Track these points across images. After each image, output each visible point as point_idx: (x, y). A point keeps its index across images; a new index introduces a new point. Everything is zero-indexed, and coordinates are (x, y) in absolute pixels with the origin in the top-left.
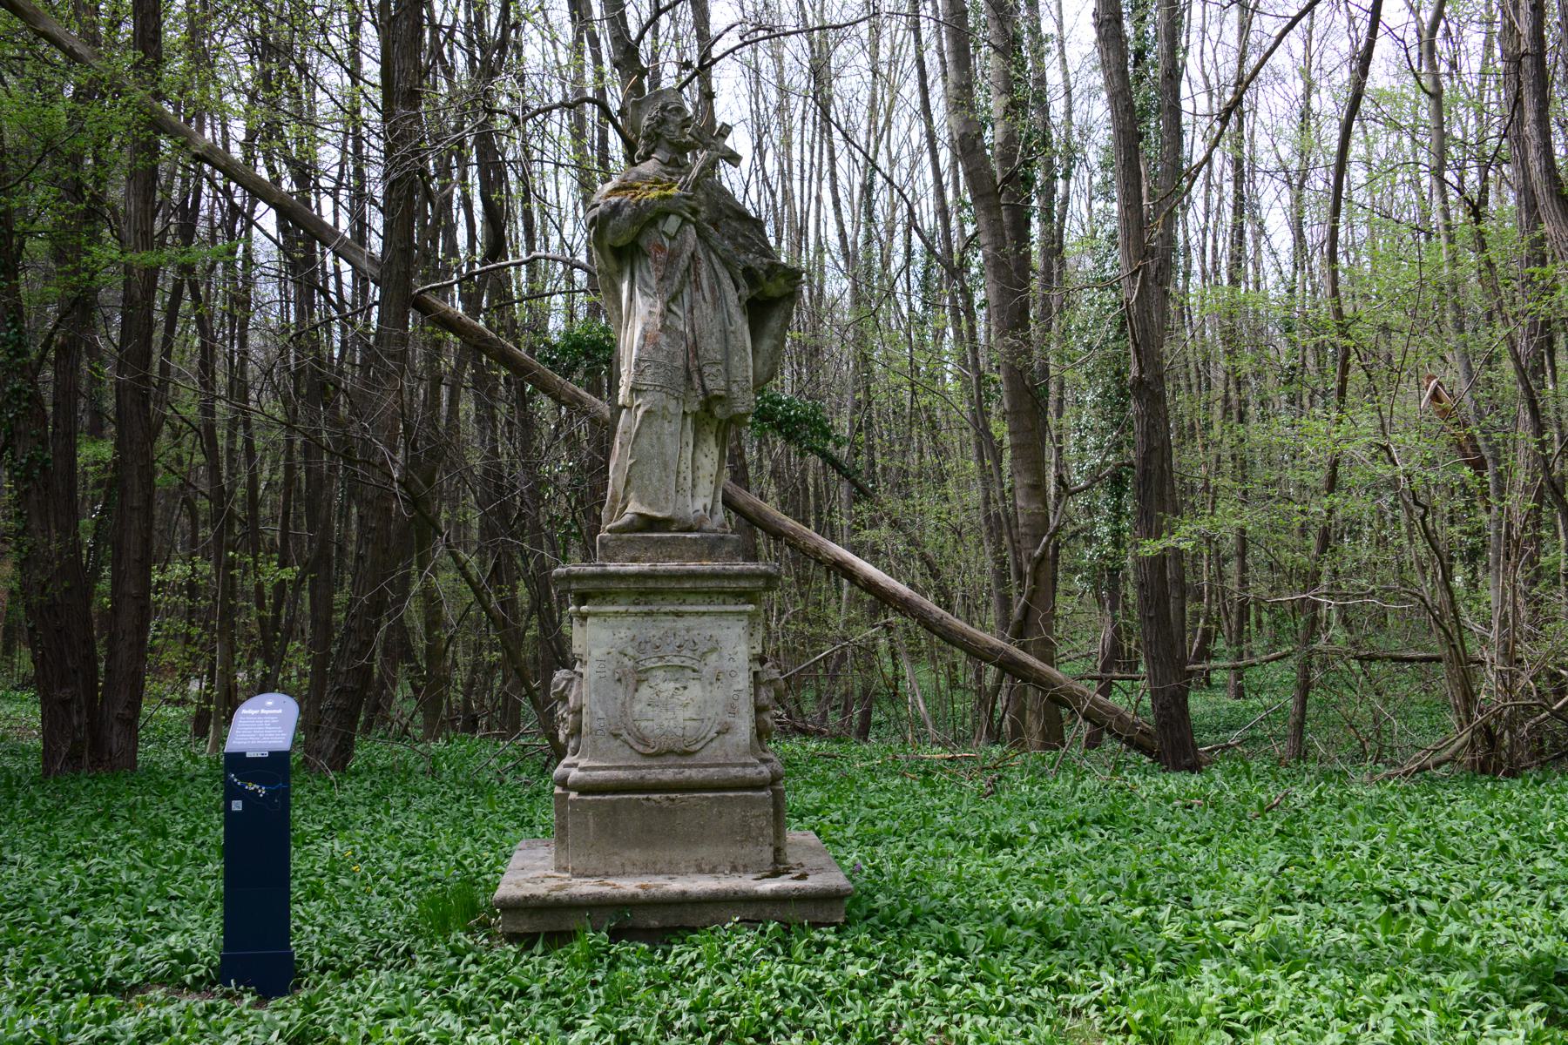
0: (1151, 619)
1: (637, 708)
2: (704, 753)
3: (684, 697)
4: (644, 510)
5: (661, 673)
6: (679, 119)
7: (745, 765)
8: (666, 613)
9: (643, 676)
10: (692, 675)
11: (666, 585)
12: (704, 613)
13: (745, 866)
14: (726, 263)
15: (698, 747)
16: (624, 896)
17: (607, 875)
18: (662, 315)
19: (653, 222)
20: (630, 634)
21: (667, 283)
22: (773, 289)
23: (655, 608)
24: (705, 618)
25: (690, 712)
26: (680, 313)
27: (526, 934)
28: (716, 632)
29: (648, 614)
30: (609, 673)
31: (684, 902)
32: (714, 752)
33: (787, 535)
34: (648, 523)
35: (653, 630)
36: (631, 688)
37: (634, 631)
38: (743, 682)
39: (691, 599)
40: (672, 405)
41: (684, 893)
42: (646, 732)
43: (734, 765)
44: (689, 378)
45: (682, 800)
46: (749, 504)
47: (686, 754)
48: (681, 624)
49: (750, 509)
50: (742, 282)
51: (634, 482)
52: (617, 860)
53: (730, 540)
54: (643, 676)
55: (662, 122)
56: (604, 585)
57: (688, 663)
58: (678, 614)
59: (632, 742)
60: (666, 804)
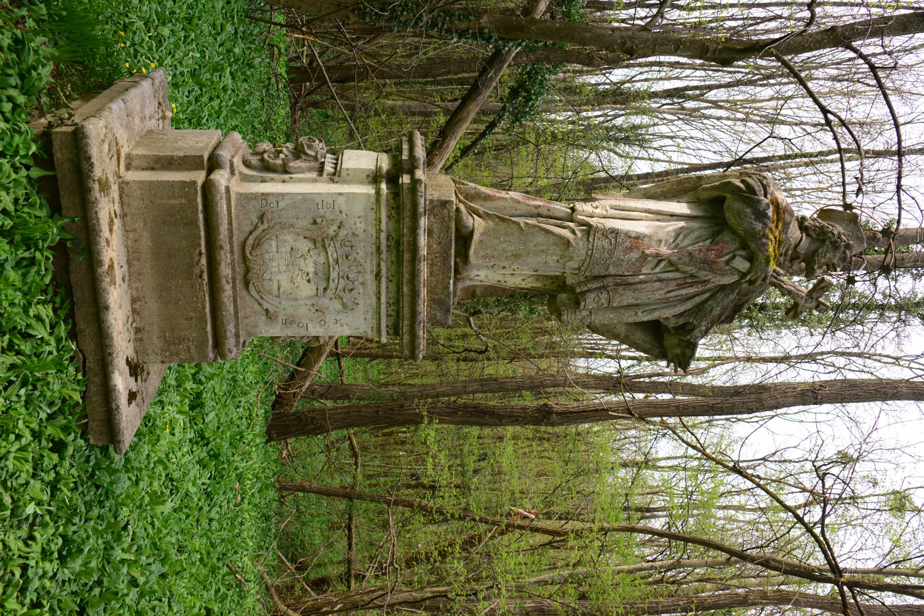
0: (377, 412)
1: (289, 238)
2: (248, 298)
3: (301, 281)
4: (476, 237)
5: (322, 259)
6: (835, 261)
7: (237, 335)
8: (379, 265)
9: (319, 245)
10: (321, 288)
11: (406, 270)
12: (379, 299)
13: (141, 340)
14: (700, 307)
15: (253, 292)
16: (98, 253)
17: (124, 216)
18: (657, 255)
19: (744, 246)
20: (360, 232)
21: (686, 259)
22: (670, 341)
23: (384, 256)
24: (374, 300)
25: (286, 285)
26: (657, 270)
27: (51, 155)
28: (361, 308)
29: (378, 248)
30: (322, 212)
31: (98, 308)
32: (249, 305)
33: (443, 142)
34: (464, 239)
35: (363, 253)
36: (308, 234)
37: (362, 236)
38: (314, 330)
39: (393, 287)
40: (574, 264)
41: (107, 308)
42: (266, 246)
43: (237, 327)
44: (596, 278)
45: (201, 285)
46: (468, 113)
47: (247, 284)
48: (369, 278)
49: (465, 114)
50: (681, 321)
51: (503, 226)
52: (139, 225)
53: (447, 318)
54: (319, 245)
55: (835, 246)
56: (407, 213)
57: (332, 285)
58: (378, 276)
59: (256, 234)
60: (197, 271)
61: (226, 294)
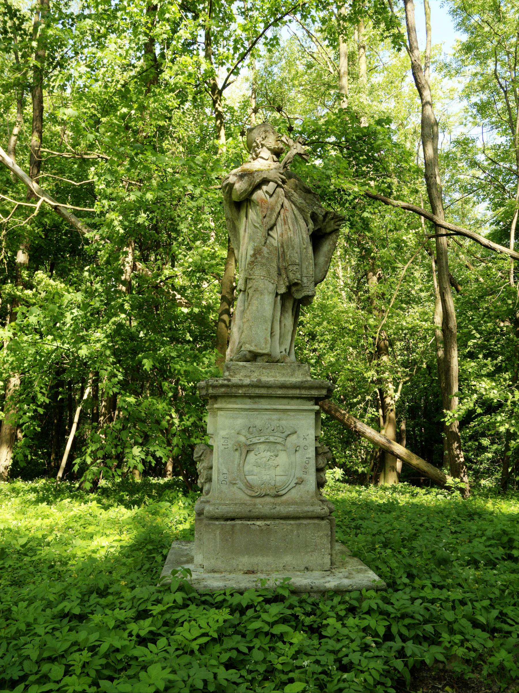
1: (247, 468)
30: (230, 446)
35: (259, 420)
50: (310, 221)
61: (282, 509)
